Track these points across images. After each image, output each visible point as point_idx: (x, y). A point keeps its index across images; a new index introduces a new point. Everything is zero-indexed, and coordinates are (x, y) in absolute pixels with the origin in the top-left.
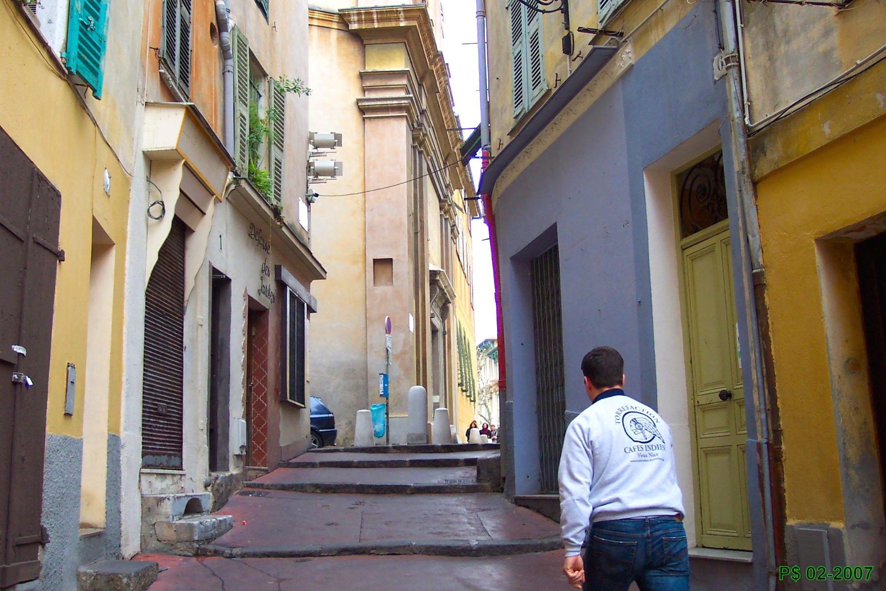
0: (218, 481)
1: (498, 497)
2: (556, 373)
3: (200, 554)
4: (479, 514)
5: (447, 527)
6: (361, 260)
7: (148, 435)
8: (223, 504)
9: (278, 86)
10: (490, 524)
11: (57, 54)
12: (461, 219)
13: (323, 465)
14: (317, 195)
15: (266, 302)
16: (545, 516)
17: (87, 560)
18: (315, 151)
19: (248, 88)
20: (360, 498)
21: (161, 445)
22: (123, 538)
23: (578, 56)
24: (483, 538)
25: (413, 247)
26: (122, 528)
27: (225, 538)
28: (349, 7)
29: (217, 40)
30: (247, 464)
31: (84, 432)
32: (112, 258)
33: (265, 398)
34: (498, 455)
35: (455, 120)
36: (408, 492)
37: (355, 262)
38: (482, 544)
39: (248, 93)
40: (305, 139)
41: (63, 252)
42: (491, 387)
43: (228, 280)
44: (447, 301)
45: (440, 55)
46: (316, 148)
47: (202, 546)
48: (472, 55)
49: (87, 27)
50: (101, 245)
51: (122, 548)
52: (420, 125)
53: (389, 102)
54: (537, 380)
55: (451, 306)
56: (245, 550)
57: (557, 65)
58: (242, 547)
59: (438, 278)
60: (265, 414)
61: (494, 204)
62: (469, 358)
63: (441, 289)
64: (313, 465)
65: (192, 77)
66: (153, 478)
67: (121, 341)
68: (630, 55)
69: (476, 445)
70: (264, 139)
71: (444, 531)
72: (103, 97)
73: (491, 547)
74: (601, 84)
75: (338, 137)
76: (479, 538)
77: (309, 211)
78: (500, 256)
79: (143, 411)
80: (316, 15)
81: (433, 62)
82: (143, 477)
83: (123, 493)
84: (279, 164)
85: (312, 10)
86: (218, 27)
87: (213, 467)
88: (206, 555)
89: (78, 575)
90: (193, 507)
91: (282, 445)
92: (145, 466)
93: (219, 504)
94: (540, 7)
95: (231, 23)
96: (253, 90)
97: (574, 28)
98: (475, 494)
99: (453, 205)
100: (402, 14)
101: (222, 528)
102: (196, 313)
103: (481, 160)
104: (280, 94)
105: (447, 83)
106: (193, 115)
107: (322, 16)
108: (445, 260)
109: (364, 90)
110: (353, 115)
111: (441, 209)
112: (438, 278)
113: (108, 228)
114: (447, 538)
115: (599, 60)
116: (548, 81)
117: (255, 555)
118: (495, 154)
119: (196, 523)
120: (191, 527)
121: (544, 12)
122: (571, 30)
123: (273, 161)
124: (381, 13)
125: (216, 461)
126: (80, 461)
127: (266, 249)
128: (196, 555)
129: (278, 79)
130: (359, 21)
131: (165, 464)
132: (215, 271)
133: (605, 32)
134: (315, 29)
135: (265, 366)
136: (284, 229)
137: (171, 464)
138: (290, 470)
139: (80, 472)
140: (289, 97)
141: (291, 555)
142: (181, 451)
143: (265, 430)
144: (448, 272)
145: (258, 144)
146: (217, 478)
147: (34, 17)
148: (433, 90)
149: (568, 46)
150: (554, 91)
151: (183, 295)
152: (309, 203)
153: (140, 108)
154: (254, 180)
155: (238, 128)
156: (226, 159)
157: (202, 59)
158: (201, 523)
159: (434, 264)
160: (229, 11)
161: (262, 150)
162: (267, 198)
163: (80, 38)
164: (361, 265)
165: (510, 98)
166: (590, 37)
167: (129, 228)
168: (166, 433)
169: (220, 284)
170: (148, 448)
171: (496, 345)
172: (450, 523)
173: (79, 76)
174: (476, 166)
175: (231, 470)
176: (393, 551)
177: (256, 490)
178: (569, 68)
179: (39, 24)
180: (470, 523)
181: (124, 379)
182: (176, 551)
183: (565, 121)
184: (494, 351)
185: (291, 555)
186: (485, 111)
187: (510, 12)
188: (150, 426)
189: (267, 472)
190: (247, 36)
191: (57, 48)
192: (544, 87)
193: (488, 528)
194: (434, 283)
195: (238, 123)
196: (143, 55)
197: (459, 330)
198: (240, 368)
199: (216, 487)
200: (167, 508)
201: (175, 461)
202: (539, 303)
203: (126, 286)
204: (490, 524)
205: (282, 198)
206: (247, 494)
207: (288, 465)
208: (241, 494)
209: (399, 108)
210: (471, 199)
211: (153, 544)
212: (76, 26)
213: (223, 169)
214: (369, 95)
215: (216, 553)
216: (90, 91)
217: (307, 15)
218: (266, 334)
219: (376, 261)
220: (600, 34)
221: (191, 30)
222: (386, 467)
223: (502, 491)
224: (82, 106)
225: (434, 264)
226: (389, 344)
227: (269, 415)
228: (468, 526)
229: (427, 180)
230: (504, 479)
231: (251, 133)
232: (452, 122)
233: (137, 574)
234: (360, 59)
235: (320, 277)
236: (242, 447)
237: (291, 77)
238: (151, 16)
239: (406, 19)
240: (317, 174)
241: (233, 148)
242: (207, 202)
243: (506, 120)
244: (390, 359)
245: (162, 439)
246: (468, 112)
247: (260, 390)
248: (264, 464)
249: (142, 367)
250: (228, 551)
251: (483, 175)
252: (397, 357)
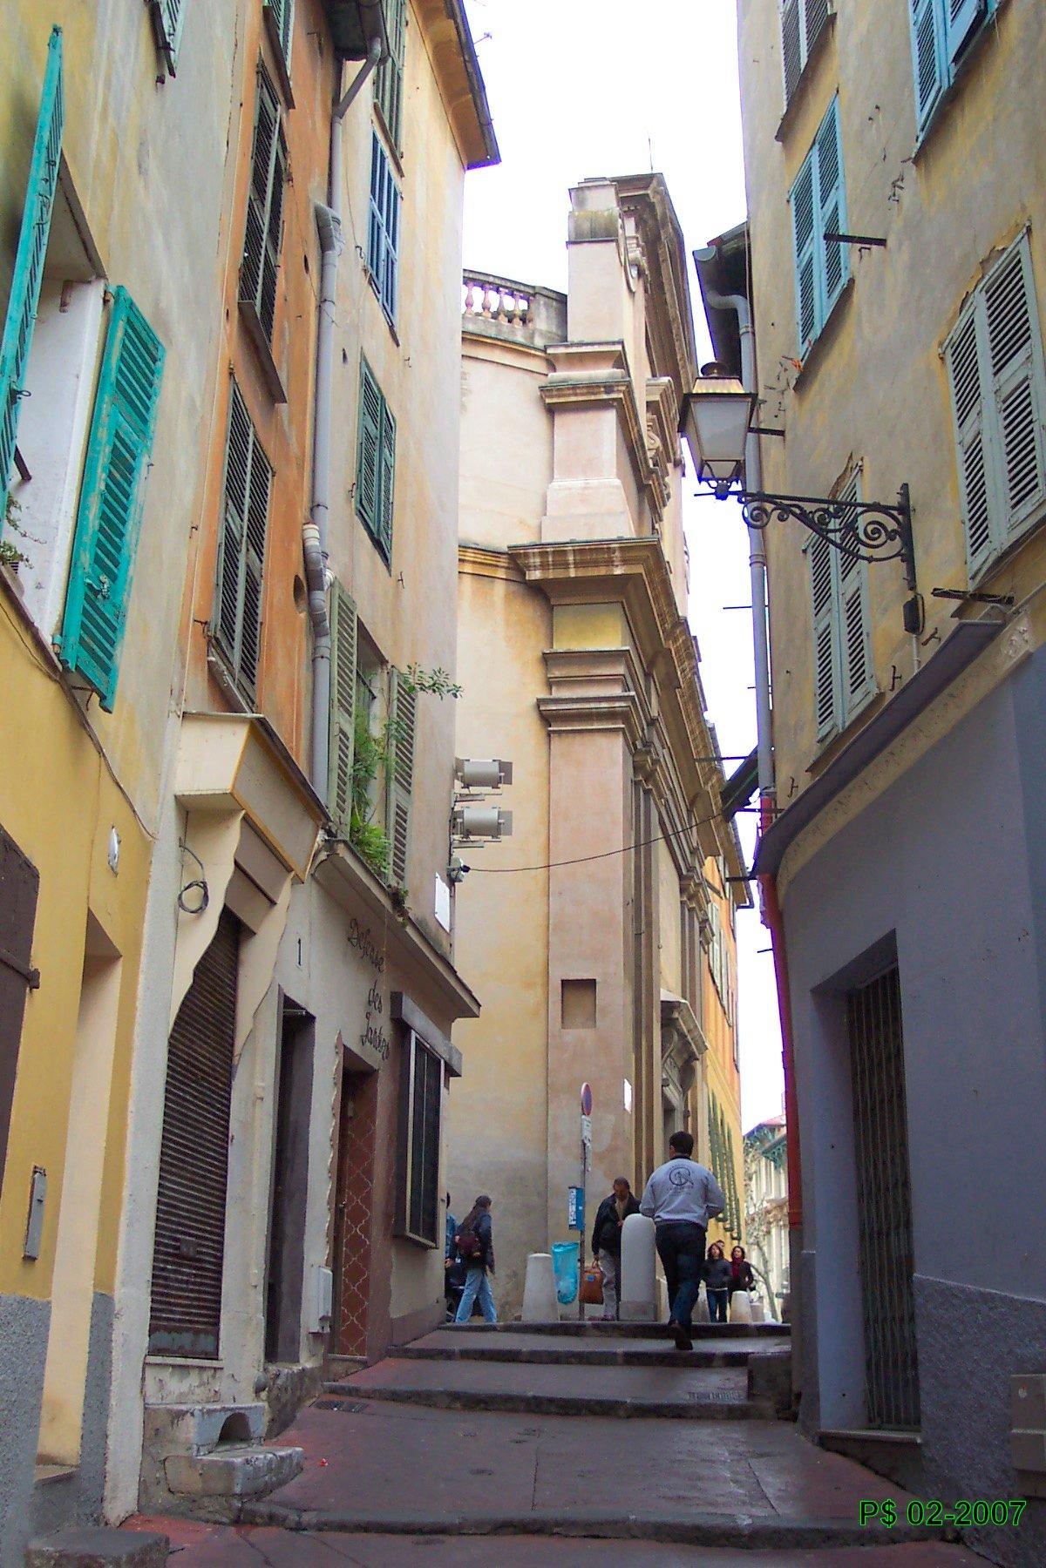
0: (279, 1382)
1: (788, 1429)
2: (895, 1202)
3: (242, 1520)
4: (754, 1462)
5: (694, 1487)
6: (540, 980)
7: (162, 1294)
8: (285, 1425)
9: (406, 682)
10: (773, 1484)
11: (47, 639)
12: (717, 909)
13: (467, 1355)
14: (466, 869)
15: (373, 1057)
16: (877, 1473)
17: (44, 1526)
18: (466, 791)
19: (354, 684)
20: (533, 1421)
21: (183, 1313)
22: (108, 1485)
23: (932, 636)
24: (761, 1512)
25: (632, 959)
26: (108, 1467)
27: (289, 1491)
28: (525, 542)
29: (303, 605)
30: (331, 1349)
31: (54, 1289)
32: (115, 980)
33: (365, 1230)
34: (787, 1348)
35: (708, 735)
36: (622, 1413)
37: (529, 986)
38: (759, 1523)
39: (353, 693)
40: (447, 774)
41: (36, 974)
42: (768, 1212)
43: (311, 1019)
44: (693, 1057)
45: (683, 624)
46: (467, 786)
47: (248, 1506)
48: (743, 627)
49: (96, 593)
50: (99, 958)
51: (105, 1504)
52: (647, 744)
53: (593, 705)
54: (860, 1212)
55: (698, 1065)
56: (325, 1517)
57: (895, 651)
58: (320, 1510)
59: (676, 1015)
60: (365, 1258)
61: (782, 892)
62: (730, 1159)
63: (682, 1036)
64: (448, 1355)
65: (260, 668)
66: (165, 1374)
67: (124, 1126)
68: (1026, 636)
69: (745, 1327)
70: (378, 772)
71: (690, 1494)
72: (115, 708)
73: (776, 1532)
74: (973, 687)
75: (506, 768)
76: (754, 1511)
77: (452, 897)
78: (794, 1005)
79: (156, 1252)
80: (470, 556)
81: (670, 635)
82: (149, 1371)
83: (113, 1402)
84: (402, 814)
85: (463, 547)
86: (308, 582)
87: (271, 1354)
88: (254, 1524)
89: (28, 1555)
90: (234, 1430)
91: (394, 1316)
92: (154, 1351)
93: (280, 1423)
94: (864, 551)
95: (329, 576)
96: (362, 688)
97: (925, 587)
98: (744, 1422)
99: (704, 883)
100: (617, 554)
101: (283, 1471)
102: (252, 1076)
103: (758, 815)
104: (407, 695)
105: (696, 672)
106: (262, 734)
108: (689, 982)
109: (550, 684)
110: (530, 727)
111: (682, 891)
112: (676, 1015)
113: (112, 929)
114: (694, 1510)
115: (969, 645)
116: (879, 678)
117: (342, 1527)
118: (784, 803)
119: (239, 1460)
120: (229, 1468)
121: (870, 560)
122: (919, 590)
123: (393, 809)
124: (581, 551)
125: (276, 1344)
126: (45, 1341)
127: (377, 963)
128: (236, 1522)
129: (405, 670)
130: (544, 566)
131: (188, 1347)
132: (288, 1003)
133: (980, 596)
134: (467, 579)
135: (369, 1173)
136: (409, 929)
137: (199, 1348)
138: (408, 1364)
139: (43, 1362)
140: (423, 698)
141: (408, 1530)
142: (217, 1324)
143: (365, 1288)
144: (693, 1004)
145: (367, 780)
146: (278, 1376)
147: (15, 579)
148: (670, 683)
149: (914, 618)
150: (890, 696)
151: (232, 1045)
152: (452, 881)
153: (174, 722)
154: (359, 843)
155: (336, 753)
156: (313, 808)
157: (278, 637)
158: (247, 1462)
159: (668, 990)
160: (326, 556)
161: (374, 792)
162: (380, 874)
163: (85, 613)
164: (539, 991)
165: (811, 707)
166: (955, 604)
167: (146, 929)
168: (192, 1291)
169: (296, 1026)
170: (159, 1318)
171: (784, 1131)
172: (700, 1479)
173: (79, 677)
174: (747, 826)
175: (304, 1355)
176: (594, 1531)
177: (346, 1399)
178: (915, 658)
179: (22, 592)
180: (736, 1482)
181: (125, 1193)
182: (202, 1513)
183: (909, 750)
184: (779, 1142)
185: (408, 1530)
186: (765, 728)
187: (810, 557)
188: (166, 1278)
189: (365, 1365)
190: (355, 597)
191: (47, 627)
192: (871, 688)
193: (769, 1492)
194: (668, 1023)
195: (336, 744)
196: (183, 631)
197: (713, 1109)
198: (326, 1175)
199: (275, 1392)
200: (189, 1430)
201: (205, 1342)
202: (863, 1072)
203: (137, 1029)
204: (773, 1484)
205: (407, 875)
206: (329, 1405)
207: (406, 1354)
208: (319, 1406)
209: (611, 715)
210: (737, 879)
211: (161, 1497)
212: (80, 591)
213: (309, 825)
214: (557, 693)
215: (272, 1519)
216: (95, 698)
217: (456, 555)
218: (371, 1114)
219: (565, 983)
220: (969, 600)
221: (262, 589)
222: (580, 1363)
223: (794, 1418)
224: (80, 721)
225: (668, 990)
226: (587, 1134)
227: (374, 1255)
228: (733, 1487)
229: (661, 849)
230: (799, 1396)
231: (356, 761)
232: (703, 739)
233: (131, 1557)
234: (543, 630)
235: (469, 1013)
236: (323, 1319)
237: (427, 667)
238: (198, 569)
239: (625, 562)
240: (467, 833)
241: (325, 789)
242: (281, 883)
243: (805, 743)
244: (589, 1161)
246: (734, 723)
247: (357, 1216)
248: (361, 1349)
249: (157, 1173)
250: (293, 1517)
251: (761, 843)
252: (600, 1157)
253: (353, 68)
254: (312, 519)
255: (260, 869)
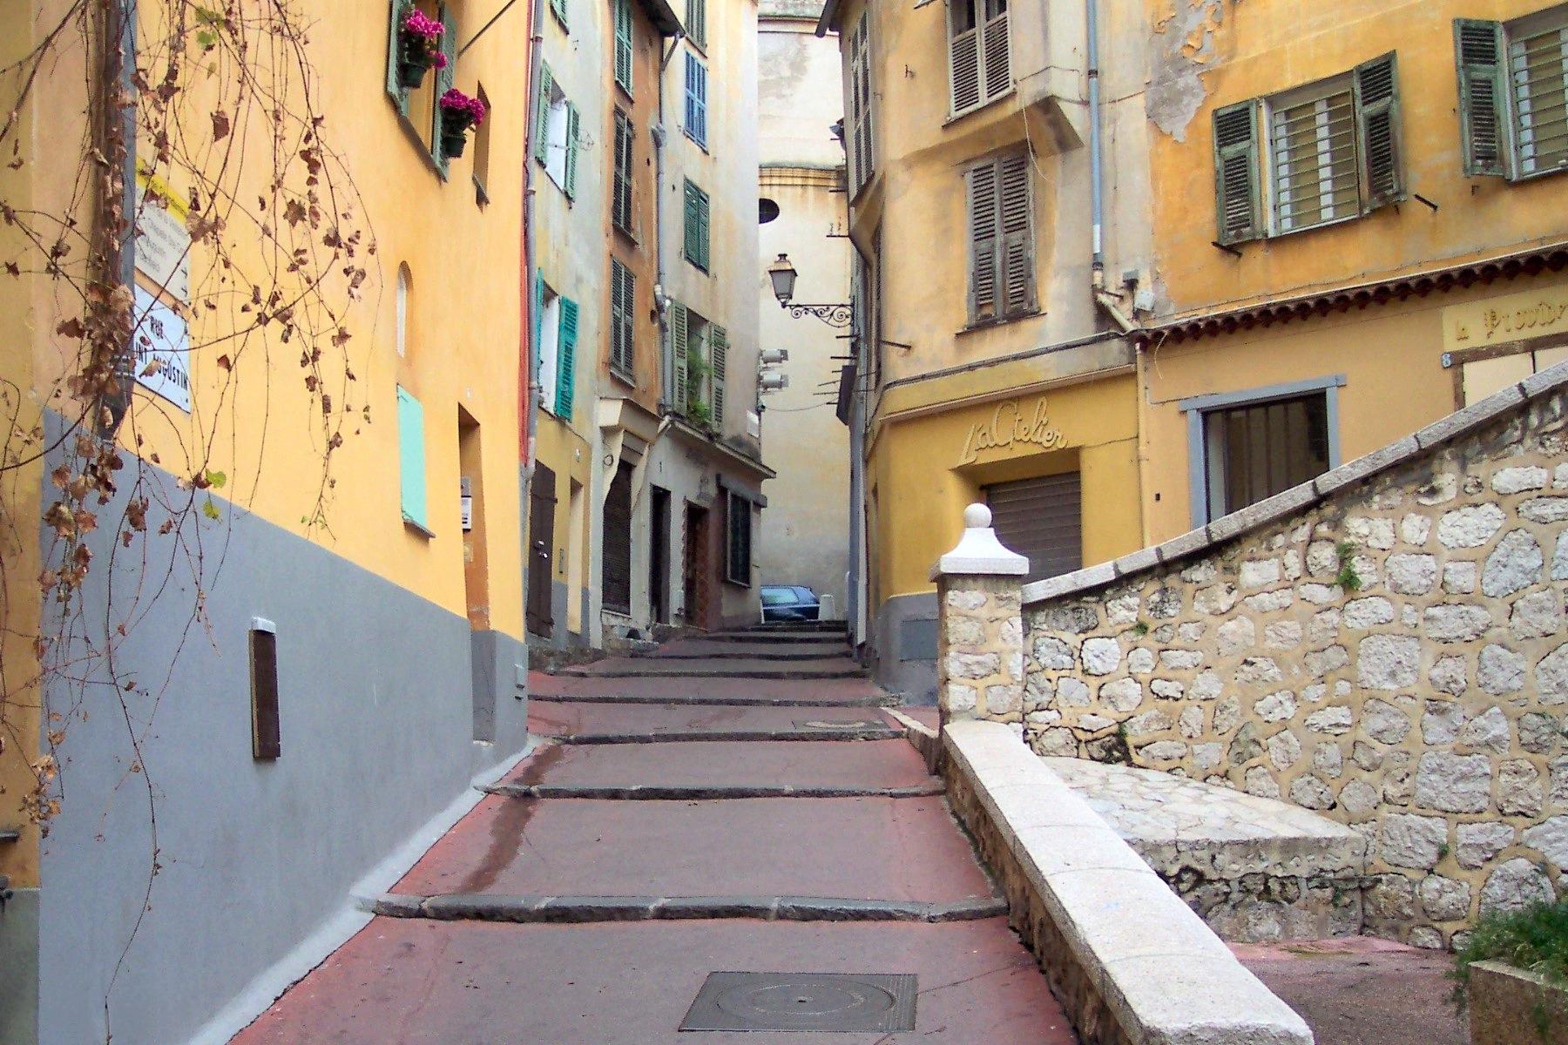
32: (582, 493)
50: (575, 487)
84: (719, 392)
107: (819, 174)
143: (707, 601)
152: (759, 413)
169: (660, 498)
200: (616, 631)
201: (624, 608)
240: (766, 387)
245: (616, 591)
253: (669, 41)
254: (659, 282)
255: (633, 444)
